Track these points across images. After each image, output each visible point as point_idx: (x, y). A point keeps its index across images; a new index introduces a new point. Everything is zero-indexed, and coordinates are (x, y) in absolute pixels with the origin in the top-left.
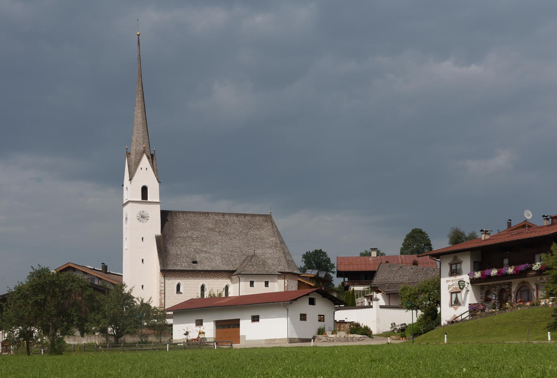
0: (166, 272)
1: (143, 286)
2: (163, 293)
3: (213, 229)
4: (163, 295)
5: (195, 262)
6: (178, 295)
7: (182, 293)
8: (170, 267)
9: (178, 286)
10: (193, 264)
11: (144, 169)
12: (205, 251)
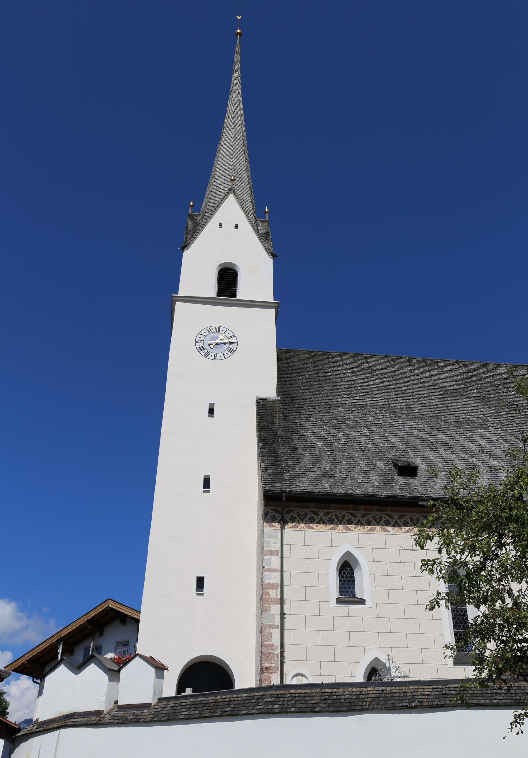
0: (283, 505)
1: (200, 581)
2: (272, 599)
3: (457, 393)
4: (275, 609)
5: (408, 470)
6: (344, 607)
7: (362, 602)
8: (307, 483)
9: (346, 570)
10: (402, 480)
11: (228, 226)
12: (445, 444)
